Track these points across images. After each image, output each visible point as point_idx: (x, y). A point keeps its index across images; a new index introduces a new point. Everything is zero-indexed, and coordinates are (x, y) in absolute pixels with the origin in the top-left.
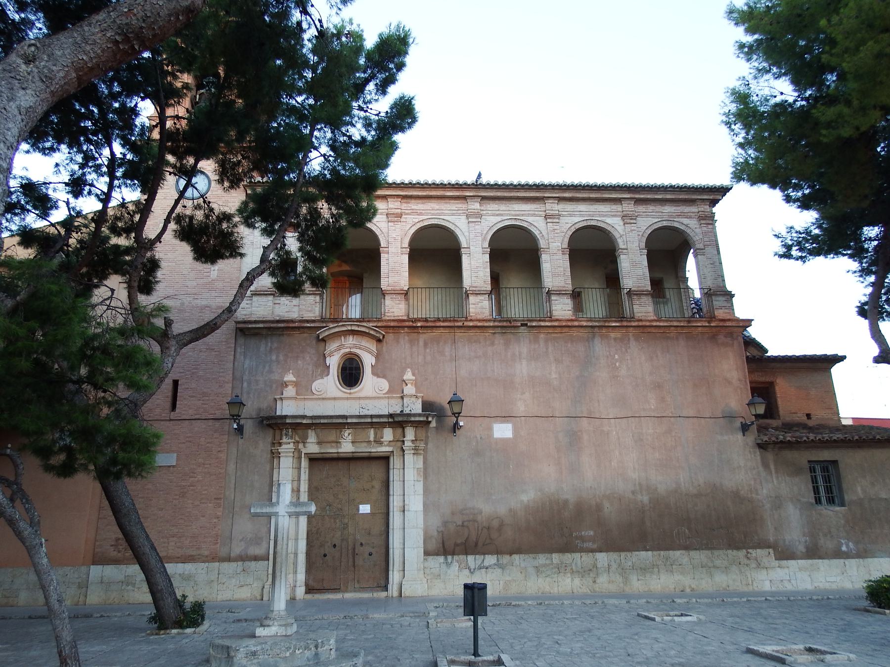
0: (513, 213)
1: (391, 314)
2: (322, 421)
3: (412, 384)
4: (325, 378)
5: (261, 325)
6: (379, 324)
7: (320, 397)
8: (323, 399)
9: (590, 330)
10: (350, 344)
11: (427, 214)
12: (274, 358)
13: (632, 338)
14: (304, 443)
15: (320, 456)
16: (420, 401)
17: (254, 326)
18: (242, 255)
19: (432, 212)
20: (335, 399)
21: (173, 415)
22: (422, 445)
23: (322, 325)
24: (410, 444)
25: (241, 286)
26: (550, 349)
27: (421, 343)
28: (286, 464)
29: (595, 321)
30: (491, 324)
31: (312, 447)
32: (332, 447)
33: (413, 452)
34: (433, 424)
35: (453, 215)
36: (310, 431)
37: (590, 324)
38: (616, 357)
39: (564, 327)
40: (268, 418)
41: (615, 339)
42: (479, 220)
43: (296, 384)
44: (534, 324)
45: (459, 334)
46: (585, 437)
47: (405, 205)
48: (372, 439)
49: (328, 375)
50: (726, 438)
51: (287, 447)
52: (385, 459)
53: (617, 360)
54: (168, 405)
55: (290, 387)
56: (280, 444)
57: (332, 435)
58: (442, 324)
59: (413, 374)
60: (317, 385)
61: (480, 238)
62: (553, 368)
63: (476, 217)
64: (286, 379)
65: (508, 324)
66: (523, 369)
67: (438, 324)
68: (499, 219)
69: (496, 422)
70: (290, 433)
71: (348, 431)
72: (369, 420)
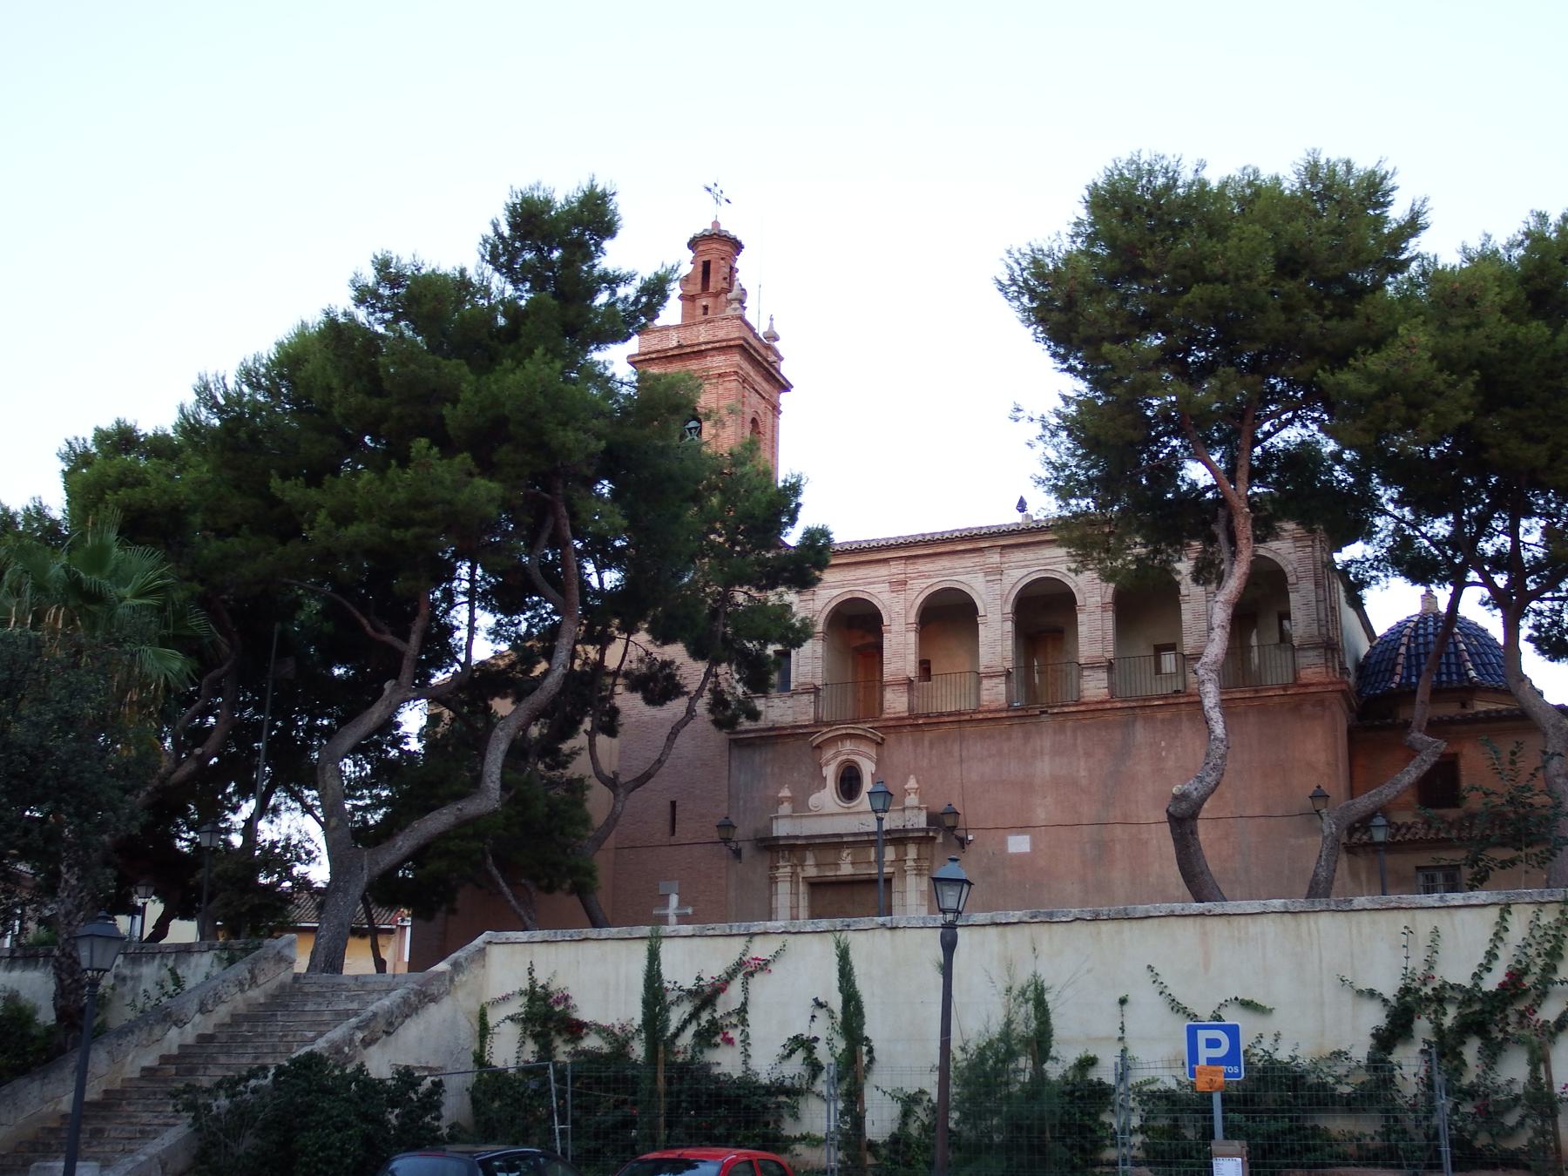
0: (1043, 562)
1: (892, 711)
2: (818, 841)
3: (916, 793)
4: (822, 791)
5: (752, 735)
6: (876, 725)
7: (851, 811)
8: (821, 815)
9: (1130, 712)
10: (847, 750)
11: (937, 576)
12: (769, 770)
13: (1185, 719)
14: (802, 866)
15: (818, 880)
16: (924, 812)
17: (745, 736)
18: (1277, 178)
19: (943, 572)
20: (832, 815)
21: (673, 840)
22: (926, 864)
23: (815, 730)
24: (912, 863)
25: (668, 739)
26: (1080, 740)
27: (926, 743)
28: (784, 888)
29: (1133, 701)
30: (1004, 715)
31: (811, 871)
32: (831, 870)
33: (915, 872)
34: (940, 840)
35: (968, 573)
36: (807, 852)
37: (1126, 705)
38: (1163, 744)
39: (1096, 711)
40: (762, 840)
41: (1163, 721)
42: (998, 577)
43: (791, 800)
44: (1055, 711)
45: (968, 729)
46: (1118, 847)
47: (911, 567)
48: (872, 859)
49: (825, 787)
50: (1302, 841)
51: (784, 871)
52: (888, 881)
53: (1163, 749)
54: (667, 829)
55: (786, 804)
56: (778, 868)
57: (830, 856)
58: (947, 719)
59: (918, 782)
60: (814, 800)
61: (999, 602)
62: (1082, 763)
63: (995, 575)
64: (780, 795)
65: (1025, 713)
66: (1045, 767)
67: (942, 720)
68: (1025, 571)
69: (1011, 834)
70: (787, 856)
71: (847, 851)
72: (866, 838)
